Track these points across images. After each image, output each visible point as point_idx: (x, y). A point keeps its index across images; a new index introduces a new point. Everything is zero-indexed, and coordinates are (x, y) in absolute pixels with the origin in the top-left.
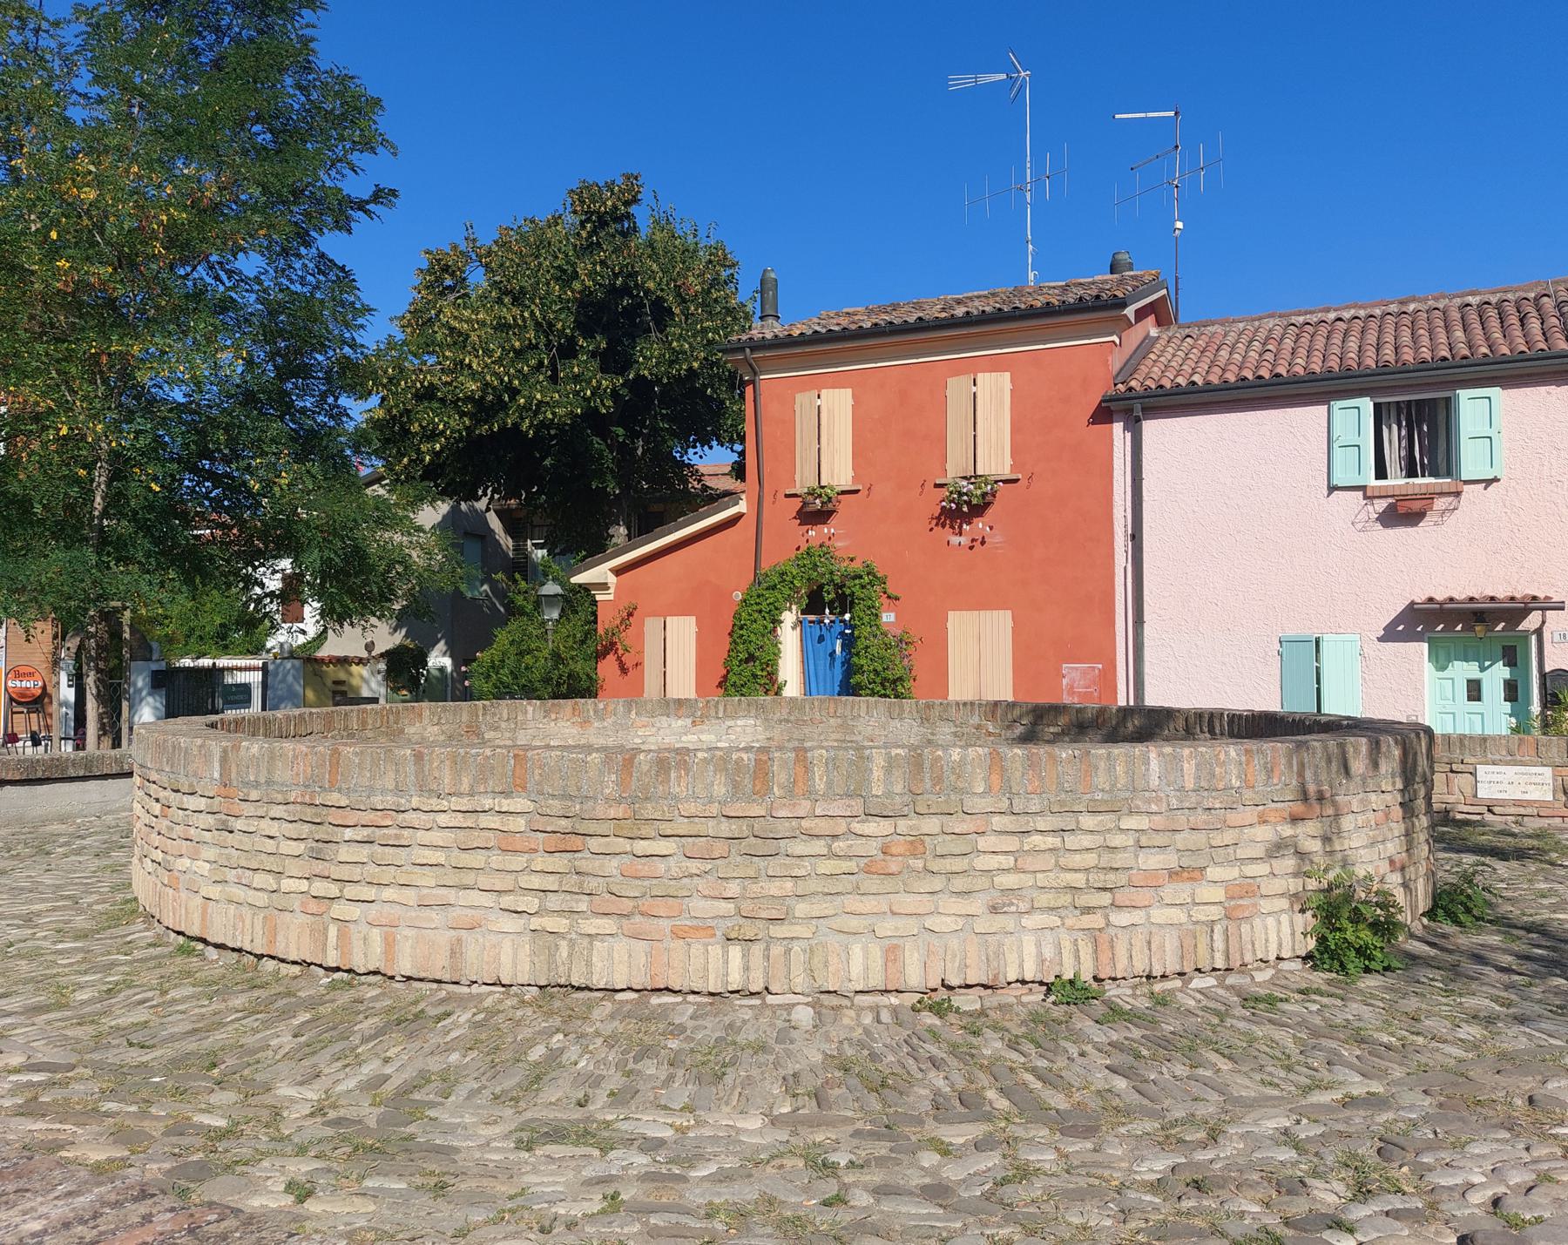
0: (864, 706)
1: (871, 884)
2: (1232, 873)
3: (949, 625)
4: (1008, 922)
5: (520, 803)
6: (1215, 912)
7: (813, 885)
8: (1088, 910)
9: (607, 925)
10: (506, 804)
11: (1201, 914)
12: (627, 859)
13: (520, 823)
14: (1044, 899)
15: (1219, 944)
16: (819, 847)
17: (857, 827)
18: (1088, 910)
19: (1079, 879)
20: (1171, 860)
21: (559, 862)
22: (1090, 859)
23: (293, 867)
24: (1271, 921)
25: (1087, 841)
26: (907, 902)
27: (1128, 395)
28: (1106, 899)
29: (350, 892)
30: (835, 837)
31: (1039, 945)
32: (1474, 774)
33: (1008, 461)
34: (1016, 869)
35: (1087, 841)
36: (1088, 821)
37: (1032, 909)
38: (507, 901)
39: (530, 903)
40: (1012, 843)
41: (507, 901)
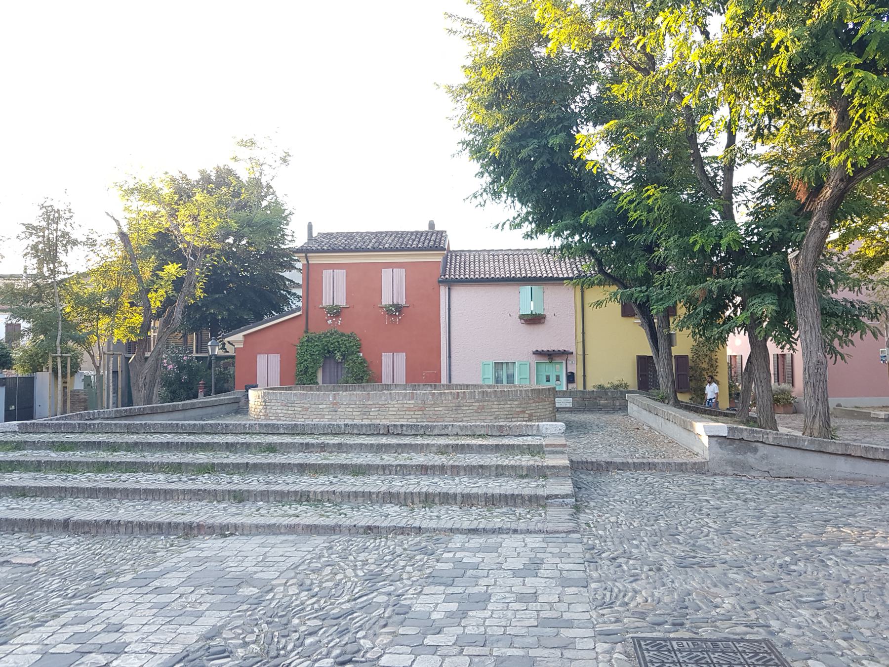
1: (475, 414)
2: (529, 412)
3: (383, 358)
5: (413, 402)
7: (466, 415)
10: (409, 402)
14: (502, 416)
16: (467, 408)
21: (420, 413)
25: (509, 406)
33: (404, 300)
35: (509, 406)
36: (509, 403)
40: (497, 407)
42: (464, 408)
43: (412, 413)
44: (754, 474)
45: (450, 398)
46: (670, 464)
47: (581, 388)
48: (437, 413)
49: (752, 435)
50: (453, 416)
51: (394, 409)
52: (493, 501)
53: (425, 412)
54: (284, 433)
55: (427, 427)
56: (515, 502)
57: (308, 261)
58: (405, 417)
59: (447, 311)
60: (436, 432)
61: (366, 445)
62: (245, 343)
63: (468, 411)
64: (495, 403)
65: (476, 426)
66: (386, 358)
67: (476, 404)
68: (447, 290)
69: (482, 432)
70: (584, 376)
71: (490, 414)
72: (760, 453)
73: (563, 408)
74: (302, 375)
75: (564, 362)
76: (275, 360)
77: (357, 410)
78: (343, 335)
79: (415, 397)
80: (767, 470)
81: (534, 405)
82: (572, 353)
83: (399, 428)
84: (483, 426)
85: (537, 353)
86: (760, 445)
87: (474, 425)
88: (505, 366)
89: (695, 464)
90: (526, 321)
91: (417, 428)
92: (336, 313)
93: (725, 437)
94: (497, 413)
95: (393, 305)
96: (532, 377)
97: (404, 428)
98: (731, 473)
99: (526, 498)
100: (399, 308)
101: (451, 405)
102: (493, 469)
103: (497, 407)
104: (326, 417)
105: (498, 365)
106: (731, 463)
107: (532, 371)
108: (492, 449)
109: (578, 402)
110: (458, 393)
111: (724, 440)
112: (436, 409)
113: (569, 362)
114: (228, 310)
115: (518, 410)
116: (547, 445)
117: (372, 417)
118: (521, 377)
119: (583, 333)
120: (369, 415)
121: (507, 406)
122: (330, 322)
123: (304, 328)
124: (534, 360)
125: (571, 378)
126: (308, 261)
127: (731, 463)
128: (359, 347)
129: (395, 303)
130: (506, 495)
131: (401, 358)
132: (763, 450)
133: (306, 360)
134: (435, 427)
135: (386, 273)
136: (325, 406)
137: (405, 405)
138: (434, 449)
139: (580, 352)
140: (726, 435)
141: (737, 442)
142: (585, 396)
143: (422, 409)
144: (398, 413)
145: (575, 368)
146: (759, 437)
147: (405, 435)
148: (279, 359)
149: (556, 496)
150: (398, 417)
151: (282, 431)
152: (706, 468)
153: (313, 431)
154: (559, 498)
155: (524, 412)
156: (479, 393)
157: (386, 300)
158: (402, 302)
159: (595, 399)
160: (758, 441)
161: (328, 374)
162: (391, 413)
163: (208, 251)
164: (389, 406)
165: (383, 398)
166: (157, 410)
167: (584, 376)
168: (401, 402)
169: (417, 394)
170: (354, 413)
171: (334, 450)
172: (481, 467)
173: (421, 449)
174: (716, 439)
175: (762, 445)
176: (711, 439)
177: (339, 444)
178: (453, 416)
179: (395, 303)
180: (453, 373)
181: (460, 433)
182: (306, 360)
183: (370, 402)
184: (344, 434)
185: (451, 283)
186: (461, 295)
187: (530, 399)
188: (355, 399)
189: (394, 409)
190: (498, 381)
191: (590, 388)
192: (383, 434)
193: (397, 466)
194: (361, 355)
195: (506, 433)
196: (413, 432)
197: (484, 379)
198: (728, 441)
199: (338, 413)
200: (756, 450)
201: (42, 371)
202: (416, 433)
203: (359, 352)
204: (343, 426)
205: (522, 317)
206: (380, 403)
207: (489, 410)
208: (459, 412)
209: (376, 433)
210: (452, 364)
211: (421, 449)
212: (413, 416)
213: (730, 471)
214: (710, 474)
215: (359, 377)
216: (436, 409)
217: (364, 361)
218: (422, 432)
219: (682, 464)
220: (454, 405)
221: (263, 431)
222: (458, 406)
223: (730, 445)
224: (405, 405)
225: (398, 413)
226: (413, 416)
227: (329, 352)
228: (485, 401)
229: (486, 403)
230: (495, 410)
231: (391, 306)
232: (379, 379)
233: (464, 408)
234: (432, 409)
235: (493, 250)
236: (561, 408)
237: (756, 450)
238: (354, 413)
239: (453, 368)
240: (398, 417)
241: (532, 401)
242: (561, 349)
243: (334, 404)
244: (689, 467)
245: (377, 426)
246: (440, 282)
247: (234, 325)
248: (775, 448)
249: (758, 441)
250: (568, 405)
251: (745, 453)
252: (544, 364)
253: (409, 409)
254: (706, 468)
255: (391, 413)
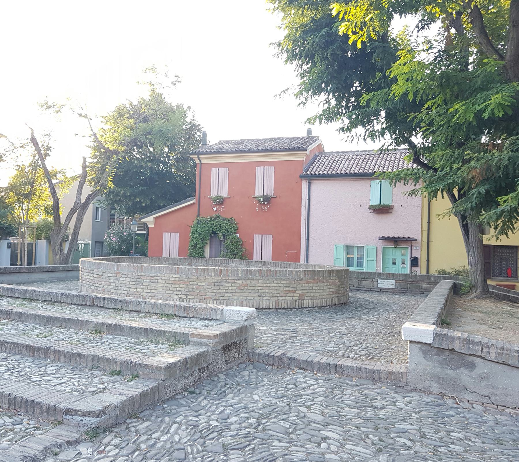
0: (232, 261)
1: (237, 291)
2: (300, 292)
3: (254, 239)
4: (261, 298)
5: (178, 276)
6: (297, 298)
7: (228, 291)
8: (275, 297)
9: (193, 297)
10: (175, 276)
11: (294, 298)
12: (196, 286)
13: (177, 279)
14: (268, 295)
15: (297, 303)
16: (230, 285)
17: (236, 281)
18: (275, 297)
19: (274, 292)
20: (289, 289)
21: (185, 286)
22: (276, 288)
23: (132, 286)
24: (307, 301)
25: (275, 285)
26: (245, 294)
27: (307, 176)
28: (278, 295)
29: (145, 291)
30: (232, 283)
31: (266, 302)
32: (377, 281)
33: (273, 192)
34: (263, 289)
35: (275, 285)
36: (275, 282)
37: (265, 296)
38: (175, 292)
39: (179, 293)
40: (262, 285)
41: (175, 292)
42: (227, 285)
43: (177, 286)
44: (467, 396)
45: (213, 275)
46: (360, 369)
47: (424, 272)
48: (200, 287)
49: (466, 346)
50: (215, 291)
51: (162, 281)
52: (15, 405)
53: (189, 286)
54: (19, 298)
55: (123, 302)
56: (34, 410)
57: (200, 161)
58: (171, 289)
59: (307, 201)
60: (131, 308)
61: (39, 316)
62: (155, 224)
63: (230, 288)
64: (260, 281)
65: (165, 305)
66: (257, 238)
67: (239, 282)
68: (308, 183)
69: (170, 312)
70: (428, 261)
71: (253, 291)
72: (477, 371)
73: (386, 289)
74: (192, 249)
75: (409, 248)
76: (175, 237)
77: (133, 280)
78: (224, 219)
79: (180, 272)
80: (486, 393)
81: (306, 285)
82: (415, 240)
83: (102, 301)
84: (171, 306)
85: (383, 239)
86: (478, 360)
87: (163, 304)
88: (355, 250)
89: (391, 373)
90: (374, 210)
91: (116, 302)
92: (219, 202)
93: (430, 344)
94: (262, 291)
95: (263, 196)
96: (378, 260)
97: (106, 301)
98: (436, 390)
99: (45, 408)
100: (267, 199)
101: (214, 281)
102: (90, 359)
103: (262, 285)
104: (112, 284)
105: (349, 249)
106: (439, 379)
107: (379, 254)
108: (141, 333)
109: (400, 285)
110: (221, 270)
111: (429, 348)
112: (199, 284)
113: (414, 248)
114: (151, 199)
115: (286, 289)
116: (193, 335)
117: (144, 287)
118: (369, 259)
119: (429, 222)
120: (142, 285)
121: (273, 285)
122: (215, 209)
123: (197, 214)
124: (381, 244)
125: (415, 262)
126: (200, 161)
127: (439, 379)
128: (236, 230)
129: (265, 194)
130: (27, 401)
131: (268, 239)
132: (482, 367)
133: (195, 238)
134: (130, 302)
135: (259, 170)
136: (111, 275)
137: (171, 279)
138: (91, 327)
139: (425, 239)
140: (431, 342)
141: (447, 353)
142: (408, 279)
143: (187, 283)
144: (165, 285)
145: (420, 253)
146: (477, 350)
147: (106, 308)
148: (178, 236)
149: (76, 412)
150: (165, 288)
151: (17, 295)
152: (404, 380)
153: (39, 298)
154: (79, 415)
155: (294, 292)
156: (243, 271)
157: (259, 192)
158: (271, 193)
159: (418, 282)
160: (474, 355)
161: (214, 250)
162: (159, 284)
163: (116, 152)
164: (158, 278)
165: (153, 271)
166: (36, 270)
167: (428, 261)
168: (168, 275)
169: (182, 268)
170: (131, 283)
171: (16, 318)
172: (80, 355)
173: (81, 325)
174: (419, 346)
175: (482, 360)
176: (413, 345)
177: (20, 312)
178: (215, 291)
179: (265, 194)
180: (310, 253)
181: (151, 311)
182: (195, 238)
183: (143, 274)
184: (60, 302)
185: (311, 178)
186: (318, 186)
187: (301, 280)
188: (132, 270)
189: (162, 281)
190: (349, 263)
191: (432, 272)
192: (89, 305)
193: (11, 343)
194: (238, 235)
195: (191, 315)
196: (113, 306)
197: (336, 260)
198: (435, 350)
199: (120, 282)
200: (472, 366)
201: (41, 239)
202: (115, 307)
203: (236, 233)
204: (60, 295)
205: (371, 207)
206: (150, 275)
207: (253, 288)
208: (221, 287)
209: (84, 304)
210: (310, 246)
211: (81, 325)
212: (178, 289)
213: (435, 388)
214: (409, 388)
215: (234, 253)
216: (199, 284)
217: (239, 240)
218: (119, 306)
219: (374, 372)
220: (216, 281)
221: (5, 294)
222: (221, 283)
223: (438, 355)
224: (171, 279)
225: (165, 285)
226: (178, 289)
227: (213, 232)
228: (249, 279)
229: (249, 281)
230: (259, 288)
231: (261, 196)
232: (251, 257)
233: (227, 285)
234: (196, 283)
235: (358, 151)
236: (384, 289)
237: (472, 366)
238: (131, 283)
239: (310, 249)
240: (165, 288)
241: (304, 282)
242: (406, 236)
243: (118, 273)
244: (383, 376)
245: (84, 297)
246: (301, 177)
247: (147, 210)
248: (501, 367)
249: (474, 355)
250: (391, 287)
251: (458, 368)
252: (391, 249)
253: (174, 282)
254: (404, 380)
255: (159, 284)
